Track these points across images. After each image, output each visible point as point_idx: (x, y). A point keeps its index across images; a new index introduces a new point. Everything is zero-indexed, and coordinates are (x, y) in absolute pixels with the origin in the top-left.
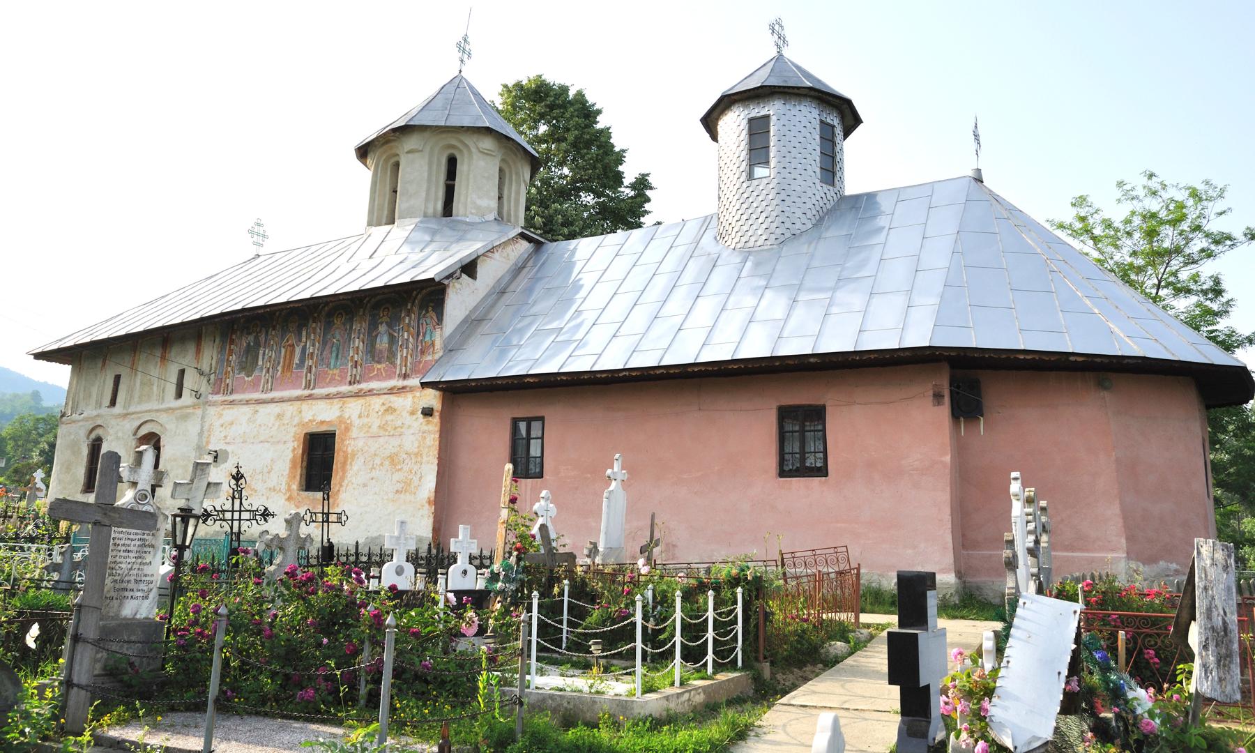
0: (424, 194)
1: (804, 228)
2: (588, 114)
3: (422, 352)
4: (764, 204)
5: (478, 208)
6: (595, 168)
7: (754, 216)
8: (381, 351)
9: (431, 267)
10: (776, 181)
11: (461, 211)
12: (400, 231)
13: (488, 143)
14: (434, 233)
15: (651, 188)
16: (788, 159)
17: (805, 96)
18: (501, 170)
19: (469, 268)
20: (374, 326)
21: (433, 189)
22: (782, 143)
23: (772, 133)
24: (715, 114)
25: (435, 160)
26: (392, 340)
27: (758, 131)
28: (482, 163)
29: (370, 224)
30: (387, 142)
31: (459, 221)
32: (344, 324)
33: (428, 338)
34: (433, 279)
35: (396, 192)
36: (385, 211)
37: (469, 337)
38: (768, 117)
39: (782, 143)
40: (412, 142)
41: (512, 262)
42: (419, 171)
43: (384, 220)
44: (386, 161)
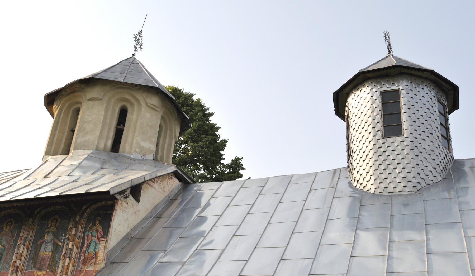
0: (98, 133)
1: (435, 180)
2: (205, 115)
3: (84, 262)
4: (400, 157)
5: (142, 148)
6: (208, 148)
7: (391, 167)
8: (43, 259)
9: (105, 183)
10: (409, 140)
11: (127, 150)
12: (77, 157)
13: (154, 101)
14: (104, 163)
15: (243, 169)
16: (418, 123)
17: (426, 79)
18: (161, 126)
19: (135, 191)
20: (40, 236)
21: (106, 130)
22: (412, 111)
23: (402, 103)
24: (347, 90)
25: (111, 108)
26: (56, 249)
27: (390, 104)
28: (148, 115)
29: (48, 153)
30: (74, 92)
31: (124, 157)
32: (12, 231)
33: (91, 249)
34: (108, 192)
35: (73, 131)
36: (61, 144)
37: (130, 251)
38: (397, 91)
39: (412, 111)
40: (95, 92)
41: (166, 194)
42: (95, 117)
43: (60, 151)
44: (69, 107)
